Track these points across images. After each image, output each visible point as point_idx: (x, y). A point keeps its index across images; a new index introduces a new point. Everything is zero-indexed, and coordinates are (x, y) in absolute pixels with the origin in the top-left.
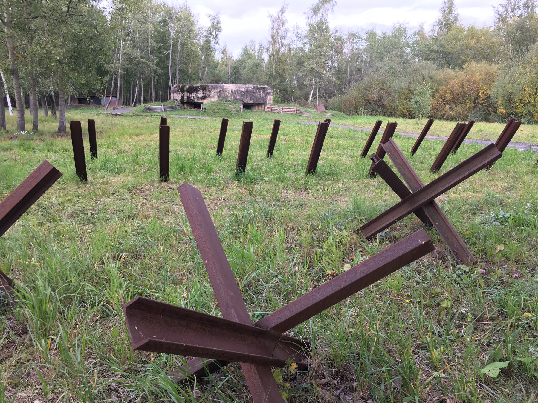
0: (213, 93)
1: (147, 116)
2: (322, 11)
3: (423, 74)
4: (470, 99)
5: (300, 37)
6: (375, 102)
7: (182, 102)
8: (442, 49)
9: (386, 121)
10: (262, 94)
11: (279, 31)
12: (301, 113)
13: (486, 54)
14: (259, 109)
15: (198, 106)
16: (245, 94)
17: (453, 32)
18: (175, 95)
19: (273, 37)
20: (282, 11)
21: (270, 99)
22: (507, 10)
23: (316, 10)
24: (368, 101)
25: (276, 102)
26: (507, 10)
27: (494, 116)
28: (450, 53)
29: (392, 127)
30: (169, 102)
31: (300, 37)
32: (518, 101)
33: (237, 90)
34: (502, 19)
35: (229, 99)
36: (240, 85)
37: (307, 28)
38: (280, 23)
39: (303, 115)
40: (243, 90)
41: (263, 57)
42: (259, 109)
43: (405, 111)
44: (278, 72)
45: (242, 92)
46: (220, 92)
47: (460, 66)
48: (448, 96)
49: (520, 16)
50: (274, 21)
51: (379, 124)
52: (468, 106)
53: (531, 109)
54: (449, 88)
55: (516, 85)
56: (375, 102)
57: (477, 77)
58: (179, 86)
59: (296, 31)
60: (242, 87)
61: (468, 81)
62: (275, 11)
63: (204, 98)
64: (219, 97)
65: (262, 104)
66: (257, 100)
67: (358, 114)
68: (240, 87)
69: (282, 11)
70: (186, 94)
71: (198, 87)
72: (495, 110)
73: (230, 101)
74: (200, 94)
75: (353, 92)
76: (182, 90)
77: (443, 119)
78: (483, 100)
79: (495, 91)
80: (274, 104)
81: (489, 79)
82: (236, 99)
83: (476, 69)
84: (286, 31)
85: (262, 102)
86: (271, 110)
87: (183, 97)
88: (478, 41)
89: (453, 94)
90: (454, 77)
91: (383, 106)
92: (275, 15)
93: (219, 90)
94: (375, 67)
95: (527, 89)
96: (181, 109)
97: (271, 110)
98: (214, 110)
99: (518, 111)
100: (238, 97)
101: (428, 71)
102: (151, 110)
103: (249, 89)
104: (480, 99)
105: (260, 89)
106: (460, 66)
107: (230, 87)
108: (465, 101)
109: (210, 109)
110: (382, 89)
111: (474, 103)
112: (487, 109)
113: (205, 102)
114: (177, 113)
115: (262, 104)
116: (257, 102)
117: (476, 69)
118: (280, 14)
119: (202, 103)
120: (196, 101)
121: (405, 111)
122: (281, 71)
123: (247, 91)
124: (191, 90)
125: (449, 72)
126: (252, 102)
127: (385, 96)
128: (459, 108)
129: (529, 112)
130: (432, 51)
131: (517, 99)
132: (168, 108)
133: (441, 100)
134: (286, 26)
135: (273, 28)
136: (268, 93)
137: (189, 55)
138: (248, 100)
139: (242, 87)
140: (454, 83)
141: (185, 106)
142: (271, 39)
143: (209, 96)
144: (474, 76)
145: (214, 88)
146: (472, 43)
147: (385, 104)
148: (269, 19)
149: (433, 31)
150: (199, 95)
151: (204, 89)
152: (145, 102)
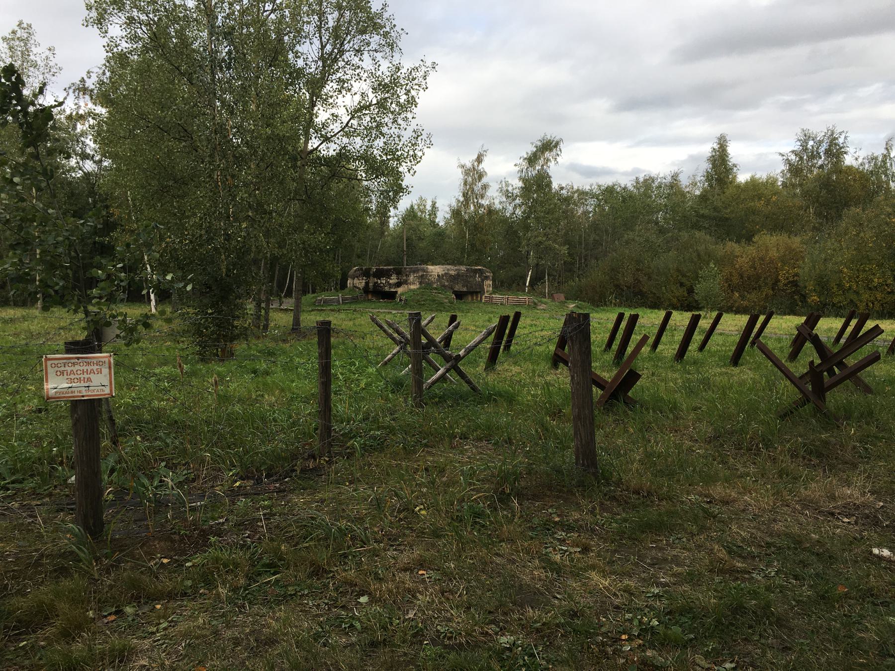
0: (411, 278)
1: (333, 310)
2: (541, 161)
3: (697, 250)
4: (766, 284)
5: (509, 196)
6: (628, 288)
7: (366, 290)
8: (715, 214)
9: (628, 313)
10: (478, 279)
11: (476, 188)
12: (535, 304)
13: (781, 221)
14: (473, 299)
15: (391, 296)
16: (454, 279)
17: (729, 191)
18: (356, 281)
19: (465, 195)
20: (479, 160)
21: (488, 284)
22: (801, 158)
23: (532, 160)
24: (617, 286)
25: (496, 288)
26: (801, 158)
27: (802, 307)
28: (727, 219)
29: (634, 319)
30: (346, 290)
31: (509, 196)
32: (835, 287)
34: (795, 170)
36: (449, 267)
37: (520, 184)
38: (476, 176)
39: (539, 308)
40: (452, 273)
41: (437, 221)
42: (473, 299)
43: (675, 301)
44: (473, 245)
45: (451, 276)
46: (422, 276)
47: (749, 239)
48: (736, 280)
49: (821, 167)
50: (467, 172)
51: (621, 317)
52: (764, 294)
53: (854, 297)
54: (736, 269)
55: (830, 265)
56: (628, 288)
57: (774, 254)
58: (362, 269)
59: (505, 189)
60: (452, 270)
61: (762, 259)
62: (469, 160)
63: (399, 285)
64: (420, 283)
65: (477, 293)
66: (471, 287)
67: (606, 305)
68: (448, 270)
69: (479, 160)
70: (373, 280)
71: (390, 270)
72: (804, 297)
73: (436, 289)
74: (393, 280)
75: (597, 274)
76: (366, 274)
77: (732, 311)
78: (785, 285)
79: (805, 270)
80: (494, 293)
81: (792, 257)
82: (444, 286)
83: (771, 243)
84: (485, 187)
86: (490, 301)
87: (367, 284)
88: (768, 202)
89: (742, 277)
90: (743, 254)
91: (641, 293)
92: (469, 165)
93: (420, 274)
94: (624, 239)
95: (845, 270)
96: (365, 301)
97: (490, 301)
98: (418, 301)
99: (835, 300)
101: (703, 247)
102: (326, 302)
104: (781, 284)
105: (476, 271)
106: (749, 239)
107: (436, 270)
108: (760, 287)
109: (413, 300)
110: (638, 270)
111: (773, 289)
112: (792, 297)
113: (400, 290)
114: (373, 306)
115: (477, 293)
116: (472, 290)
117: (771, 243)
118: (476, 164)
119: (396, 292)
120: (387, 289)
121: (675, 301)
122: (478, 244)
123: (458, 275)
124: (380, 274)
125: (732, 247)
126: (465, 289)
127: (644, 279)
128: (753, 296)
129: (852, 301)
130: (703, 216)
131: (833, 284)
132: (347, 299)
133: (726, 285)
134: (484, 180)
135: (465, 184)
136: (487, 278)
137: (358, 224)
138: (458, 287)
139: (452, 270)
140: (743, 262)
141: (370, 297)
142: (462, 199)
143: (406, 282)
144: (770, 253)
145: (414, 272)
146: (759, 204)
147: (644, 290)
148: (460, 170)
149: (694, 184)
150: (391, 282)
151: (399, 273)
152: (314, 292)
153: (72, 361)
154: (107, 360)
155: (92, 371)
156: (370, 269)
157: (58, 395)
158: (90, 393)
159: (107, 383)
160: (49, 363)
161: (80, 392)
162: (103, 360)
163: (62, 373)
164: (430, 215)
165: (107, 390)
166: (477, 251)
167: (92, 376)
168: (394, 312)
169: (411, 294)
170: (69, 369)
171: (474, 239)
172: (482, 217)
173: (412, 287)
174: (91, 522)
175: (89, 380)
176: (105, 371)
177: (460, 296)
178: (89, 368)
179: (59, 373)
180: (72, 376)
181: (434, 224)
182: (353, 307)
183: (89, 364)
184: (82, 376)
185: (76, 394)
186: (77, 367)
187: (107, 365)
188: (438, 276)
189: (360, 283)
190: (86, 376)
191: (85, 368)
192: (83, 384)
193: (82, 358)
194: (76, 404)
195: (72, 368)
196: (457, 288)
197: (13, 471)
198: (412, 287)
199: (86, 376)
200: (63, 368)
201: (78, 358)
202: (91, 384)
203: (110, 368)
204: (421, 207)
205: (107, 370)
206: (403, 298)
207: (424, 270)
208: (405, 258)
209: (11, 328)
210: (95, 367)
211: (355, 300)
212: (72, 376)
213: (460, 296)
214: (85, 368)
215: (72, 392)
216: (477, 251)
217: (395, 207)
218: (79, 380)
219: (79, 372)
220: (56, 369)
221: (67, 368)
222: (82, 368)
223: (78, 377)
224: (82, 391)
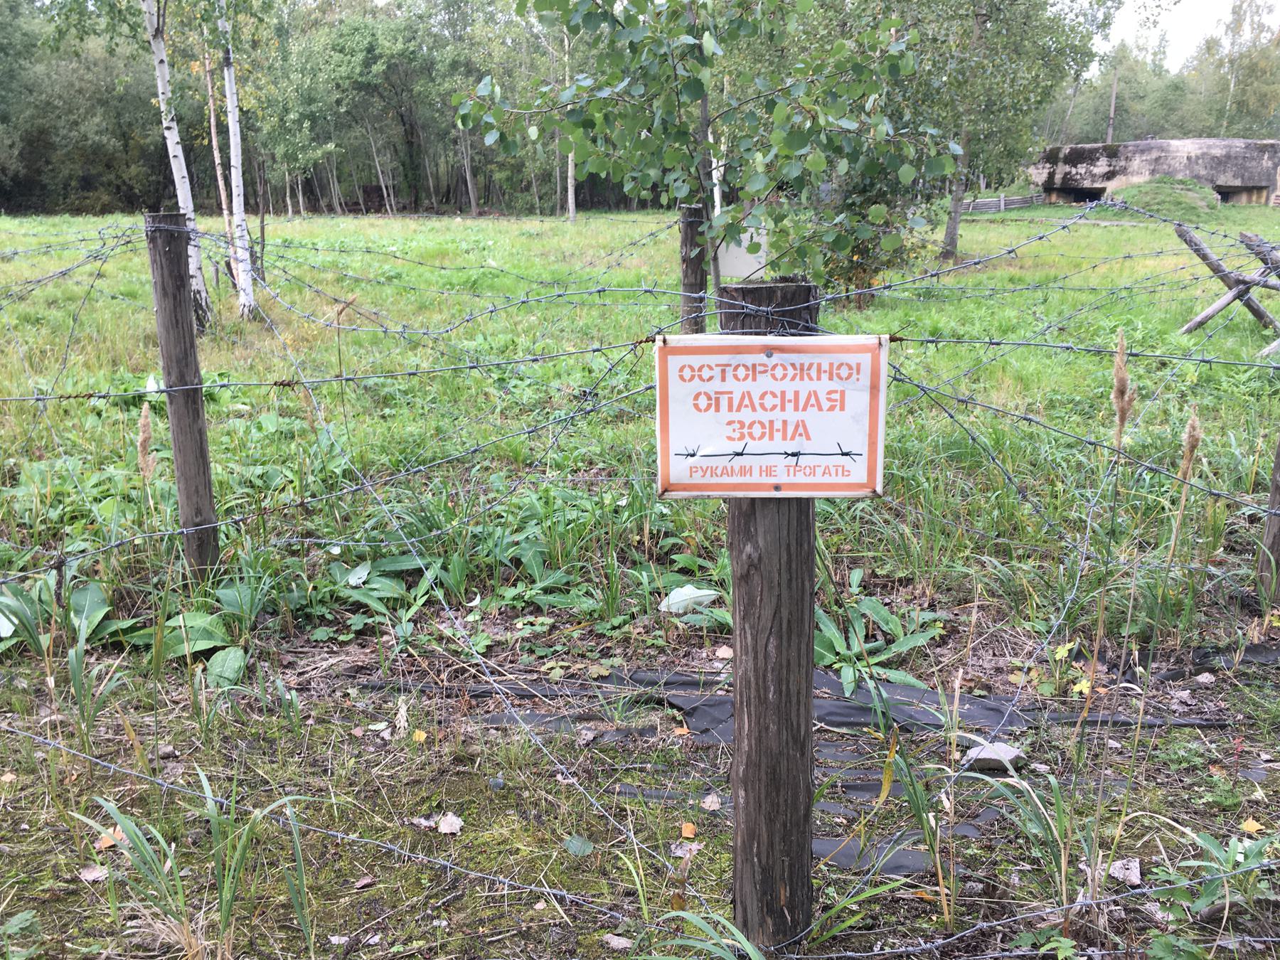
1: (992, 222)
7: (1049, 187)
14: (1250, 201)
16: (1220, 163)
33: (1204, 154)
35: (1180, 177)
36: (1211, 141)
40: (1217, 152)
42: (1250, 201)
44: (1241, 104)
45: (1213, 158)
46: (1157, 159)
63: (1110, 176)
64: (1153, 172)
65: (1260, 189)
68: (1209, 147)
70: (1062, 169)
71: (1097, 150)
73: (1181, 182)
74: (1102, 166)
82: (1198, 177)
85: (1264, 184)
87: (1051, 175)
93: (1154, 155)
96: (1044, 204)
100: (1203, 172)
103: (1233, 151)
105: (1262, 149)
107: (1184, 148)
113: (1111, 186)
116: (1251, 184)
119: (1103, 190)
120: (1087, 184)
123: (1228, 156)
124: (1076, 158)
126: (1238, 183)
132: (1013, 202)
138: (1227, 179)
139: (1217, 147)
143: (1124, 171)
145: (1142, 152)
151: (1112, 153)
153: (750, 359)
154: (865, 360)
155: (813, 400)
156: (1059, 149)
157: (697, 479)
158: (800, 478)
159: (858, 443)
160: (675, 362)
161: (769, 471)
162: (852, 359)
163: (714, 402)
164: (1155, 54)
165: (858, 472)
166: (1248, 113)
167: (811, 417)
168: (1103, 224)
169: (1135, 192)
170: (736, 388)
171: (1244, 92)
172: (1264, 53)
173: (1136, 180)
174: (784, 894)
175: (802, 430)
176: (858, 399)
177: (1226, 194)
178: (805, 387)
179: (703, 402)
180: (746, 415)
181: (1158, 71)
182: (1027, 215)
183: (802, 371)
184: (778, 416)
185: (755, 478)
186: (765, 383)
187: (865, 379)
188: (1189, 158)
189: (1039, 174)
190: (791, 416)
191: (789, 387)
192: (779, 445)
193: (782, 349)
194: (747, 513)
195: (748, 385)
196: (1222, 181)
197: (549, 563)
198: (1136, 180)
199: (791, 416)
200: (717, 385)
201: (769, 351)
202: (806, 447)
203: (874, 389)
204: (1141, 42)
205: (866, 397)
206: (1118, 199)
207: (1162, 149)
208: (1110, 131)
209: (537, 245)
210: (823, 386)
211: (1027, 204)
212: (746, 415)
213: (1226, 194)
214: (789, 387)
215: (743, 471)
216: (1248, 113)
217: (1106, 37)
218: (769, 430)
219: (769, 401)
220: (696, 385)
221: (731, 384)
222: (777, 387)
223: (765, 417)
224: (770, 474)
